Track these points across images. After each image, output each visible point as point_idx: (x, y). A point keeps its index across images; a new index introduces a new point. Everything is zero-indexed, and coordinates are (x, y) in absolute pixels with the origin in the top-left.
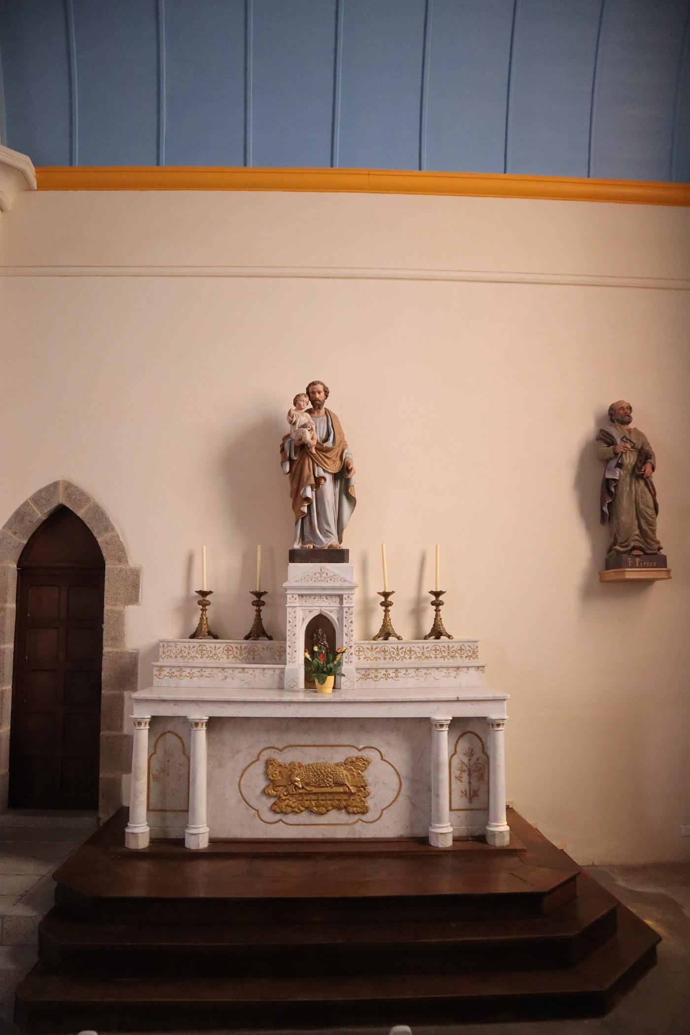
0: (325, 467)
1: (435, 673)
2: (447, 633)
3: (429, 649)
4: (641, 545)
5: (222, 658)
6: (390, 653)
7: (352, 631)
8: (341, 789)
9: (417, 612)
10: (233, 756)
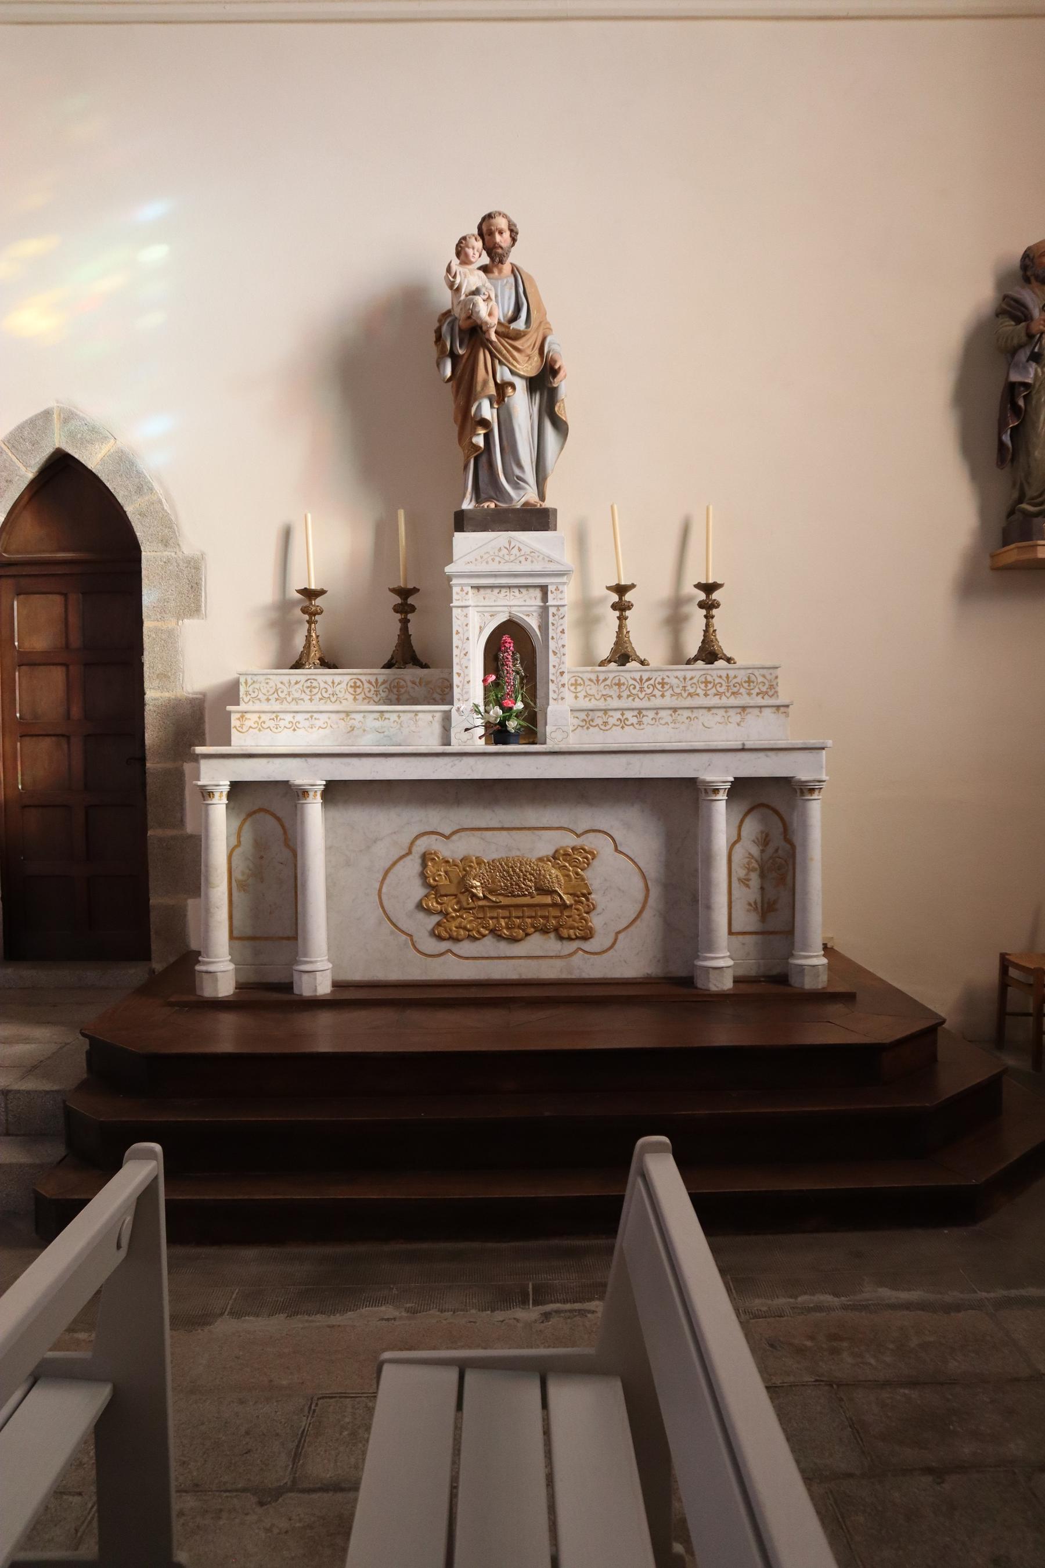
0: (513, 365)
1: (705, 717)
2: (725, 655)
3: (695, 681)
5: (346, 699)
6: (628, 687)
7: (563, 646)
8: (548, 900)
9: (675, 621)
10: (369, 847)
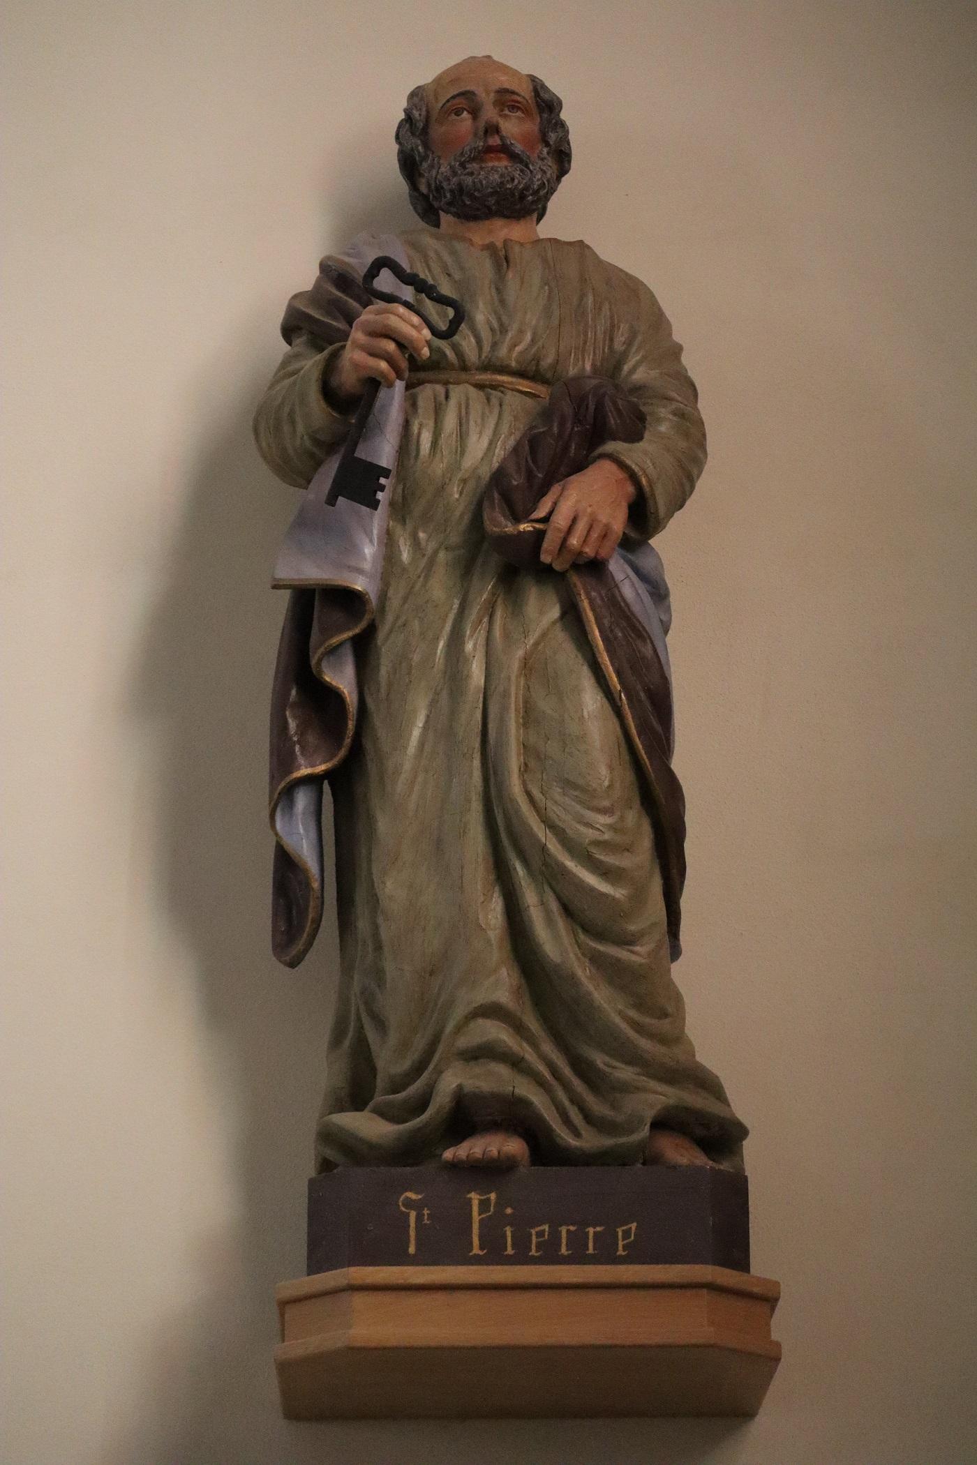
4: (525, 1089)
